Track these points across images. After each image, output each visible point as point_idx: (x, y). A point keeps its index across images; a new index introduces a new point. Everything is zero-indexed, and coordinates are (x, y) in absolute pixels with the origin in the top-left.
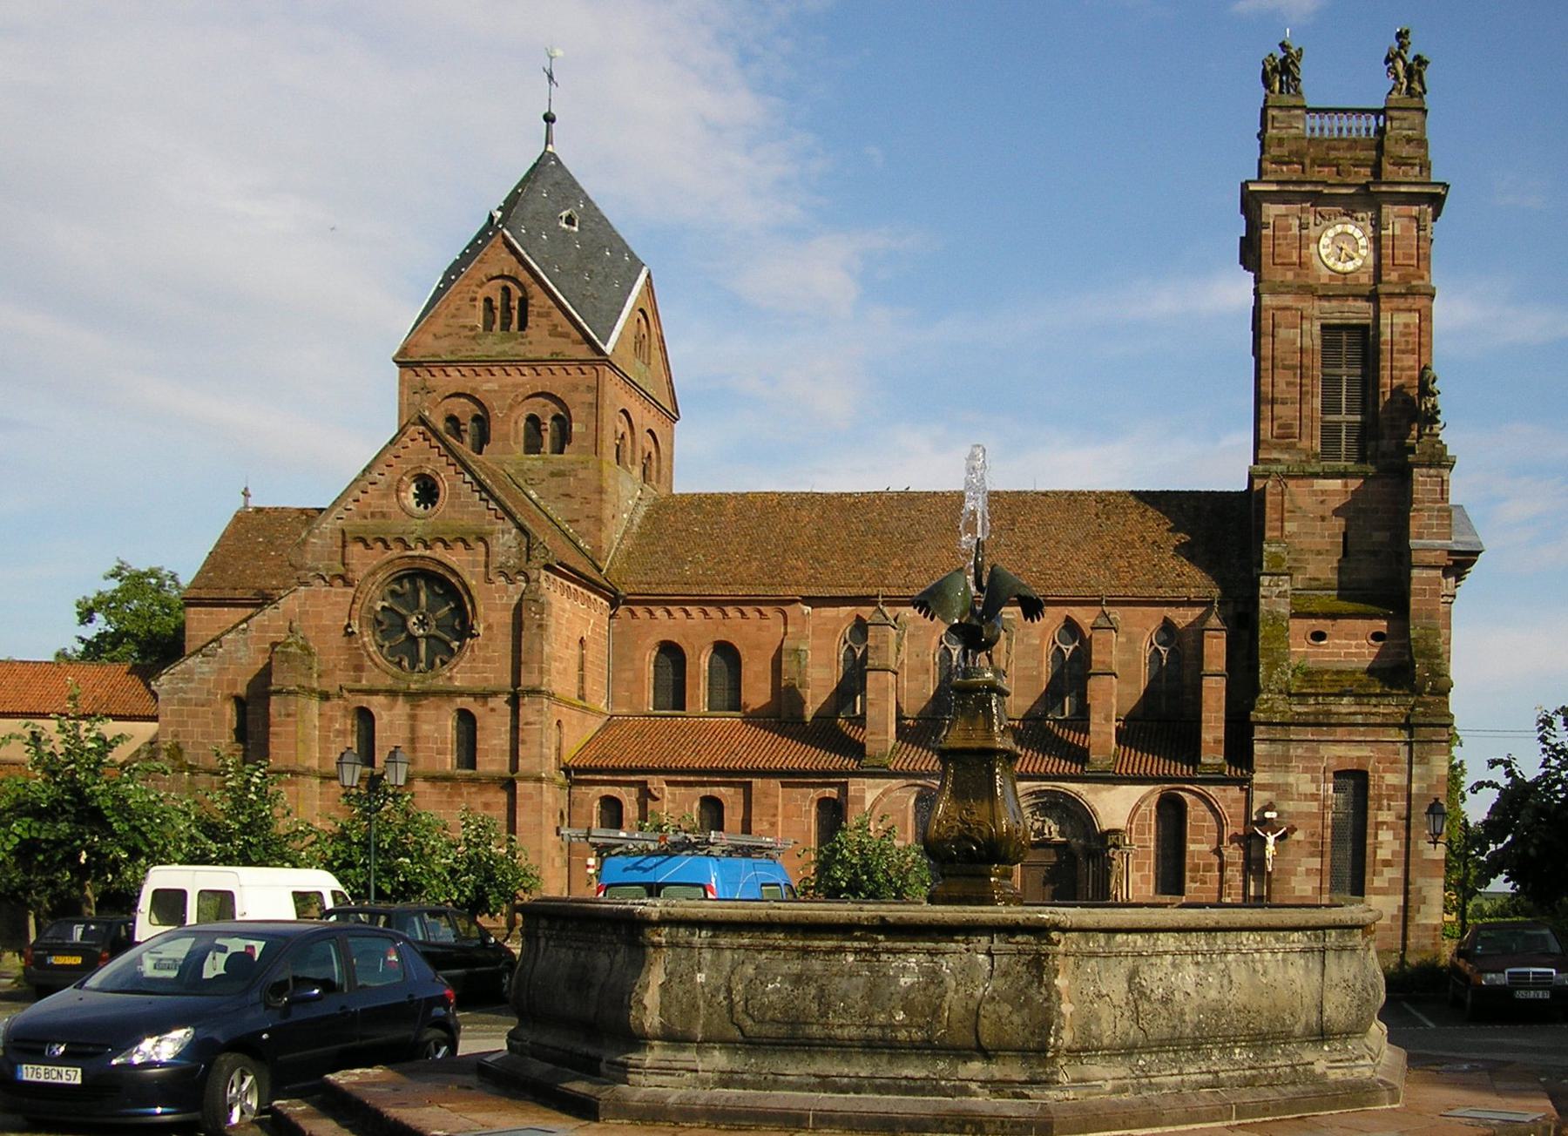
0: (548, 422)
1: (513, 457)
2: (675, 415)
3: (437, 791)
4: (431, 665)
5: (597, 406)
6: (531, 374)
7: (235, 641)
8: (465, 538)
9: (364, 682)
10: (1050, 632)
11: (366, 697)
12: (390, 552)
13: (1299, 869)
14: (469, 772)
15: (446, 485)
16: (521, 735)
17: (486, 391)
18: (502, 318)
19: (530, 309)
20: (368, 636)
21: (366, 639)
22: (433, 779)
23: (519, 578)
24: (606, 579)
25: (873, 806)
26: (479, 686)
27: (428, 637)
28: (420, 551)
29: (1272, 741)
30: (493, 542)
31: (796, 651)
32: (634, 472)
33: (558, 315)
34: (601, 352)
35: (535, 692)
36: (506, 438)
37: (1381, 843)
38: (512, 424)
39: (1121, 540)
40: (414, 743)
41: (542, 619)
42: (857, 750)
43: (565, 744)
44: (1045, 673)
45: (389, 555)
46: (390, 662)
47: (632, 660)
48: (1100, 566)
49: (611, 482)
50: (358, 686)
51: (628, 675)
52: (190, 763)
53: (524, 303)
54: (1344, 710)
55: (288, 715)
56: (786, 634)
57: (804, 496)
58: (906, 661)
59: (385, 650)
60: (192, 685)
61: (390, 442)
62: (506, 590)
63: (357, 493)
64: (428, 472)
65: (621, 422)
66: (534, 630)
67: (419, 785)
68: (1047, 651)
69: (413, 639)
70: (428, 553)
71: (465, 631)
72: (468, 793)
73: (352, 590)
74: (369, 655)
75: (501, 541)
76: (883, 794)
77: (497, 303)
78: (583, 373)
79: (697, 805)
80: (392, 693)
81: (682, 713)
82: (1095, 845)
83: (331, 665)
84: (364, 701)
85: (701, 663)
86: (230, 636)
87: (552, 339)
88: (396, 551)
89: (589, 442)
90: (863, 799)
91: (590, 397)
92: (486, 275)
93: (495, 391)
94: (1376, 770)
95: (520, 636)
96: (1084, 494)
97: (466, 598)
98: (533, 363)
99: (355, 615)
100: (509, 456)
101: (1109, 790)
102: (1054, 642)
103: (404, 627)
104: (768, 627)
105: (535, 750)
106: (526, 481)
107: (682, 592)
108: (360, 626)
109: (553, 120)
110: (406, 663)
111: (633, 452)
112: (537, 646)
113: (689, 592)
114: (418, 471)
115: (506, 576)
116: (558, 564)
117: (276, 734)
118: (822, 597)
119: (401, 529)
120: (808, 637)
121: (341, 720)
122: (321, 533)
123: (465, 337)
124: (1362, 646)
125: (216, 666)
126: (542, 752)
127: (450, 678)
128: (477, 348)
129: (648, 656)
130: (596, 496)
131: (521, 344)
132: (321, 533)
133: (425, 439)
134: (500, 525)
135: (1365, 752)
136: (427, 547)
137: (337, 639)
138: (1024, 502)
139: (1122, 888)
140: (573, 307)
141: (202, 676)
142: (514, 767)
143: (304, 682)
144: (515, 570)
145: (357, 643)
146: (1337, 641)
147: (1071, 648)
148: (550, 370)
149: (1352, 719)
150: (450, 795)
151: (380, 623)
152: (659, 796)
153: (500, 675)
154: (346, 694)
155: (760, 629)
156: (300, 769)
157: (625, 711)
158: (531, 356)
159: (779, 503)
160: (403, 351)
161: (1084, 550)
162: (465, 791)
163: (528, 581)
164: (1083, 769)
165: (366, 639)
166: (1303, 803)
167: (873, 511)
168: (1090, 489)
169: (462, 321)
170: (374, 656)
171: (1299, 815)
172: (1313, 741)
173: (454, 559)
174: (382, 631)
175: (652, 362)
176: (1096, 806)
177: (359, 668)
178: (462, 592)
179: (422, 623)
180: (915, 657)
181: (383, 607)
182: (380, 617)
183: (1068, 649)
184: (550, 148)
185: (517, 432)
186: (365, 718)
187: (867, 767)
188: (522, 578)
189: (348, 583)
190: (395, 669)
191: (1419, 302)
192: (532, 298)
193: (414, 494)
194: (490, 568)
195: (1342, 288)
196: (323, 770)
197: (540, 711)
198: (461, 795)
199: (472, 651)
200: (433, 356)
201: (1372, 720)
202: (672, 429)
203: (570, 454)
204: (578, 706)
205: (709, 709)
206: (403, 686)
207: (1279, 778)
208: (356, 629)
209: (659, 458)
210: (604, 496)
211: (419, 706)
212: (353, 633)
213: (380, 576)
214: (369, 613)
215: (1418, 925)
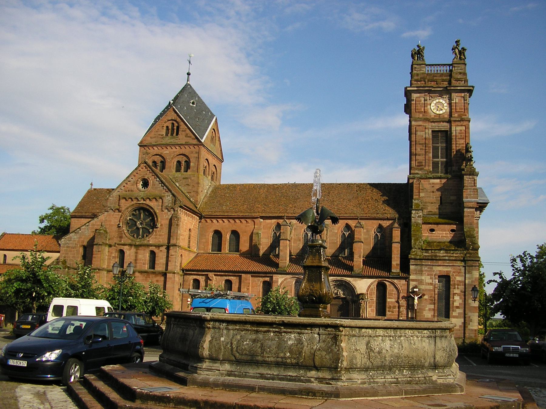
0: (183, 163)
4: (143, 237)
9: (122, 242)
10: (341, 228)
12: (133, 202)
13: (426, 308)
14: (152, 270)
16: (169, 259)
18: (171, 132)
19: (180, 129)
21: (124, 228)
22: (141, 272)
25: (281, 284)
26: (157, 244)
27: (143, 228)
28: (142, 202)
29: (416, 265)
31: (258, 233)
33: (188, 131)
34: (201, 142)
35: (175, 245)
36: (170, 167)
37: (455, 300)
38: (172, 163)
41: (178, 223)
42: (276, 265)
43: (183, 262)
44: (339, 241)
46: (131, 235)
48: (357, 207)
50: (120, 243)
51: (204, 240)
53: (178, 128)
54: (441, 255)
55: (99, 252)
56: (254, 228)
61: (135, 169)
63: (125, 184)
64: (146, 178)
66: (175, 226)
67: (137, 274)
68: (340, 234)
69: (138, 229)
70: (144, 202)
71: (154, 226)
72: (152, 277)
73: (121, 214)
74: (124, 233)
76: (284, 280)
77: (170, 128)
80: (130, 245)
81: (220, 253)
84: (122, 247)
85: (227, 237)
86: (83, 227)
88: (135, 202)
89: (195, 169)
91: (196, 155)
94: (453, 275)
96: (352, 184)
97: (155, 216)
98: (180, 145)
99: (121, 221)
101: (360, 280)
102: (342, 231)
103: (136, 225)
104: (249, 226)
108: (122, 224)
109: (190, 75)
110: (135, 236)
111: (209, 171)
114: (143, 178)
117: (95, 257)
118: (266, 216)
119: (137, 195)
121: (114, 253)
122: (113, 196)
124: (448, 234)
125: (78, 236)
130: (197, 185)
131: (177, 139)
132: (113, 196)
133: (146, 168)
134: (167, 194)
135: (449, 269)
136: (144, 200)
137: (115, 228)
138: (333, 187)
139: (364, 313)
142: (167, 269)
144: (171, 208)
146: (439, 232)
147: (348, 233)
149: (444, 258)
150: (146, 278)
151: (128, 224)
152: (212, 279)
153: (164, 240)
155: (246, 226)
156: (101, 268)
157: (202, 252)
158: (179, 143)
160: (141, 142)
161: (352, 202)
163: (174, 211)
164: (351, 273)
165: (124, 228)
166: (427, 286)
167: (283, 190)
168: (355, 183)
169: (159, 133)
170: (126, 234)
171: (426, 290)
172: (431, 265)
174: (129, 226)
178: (154, 214)
179: (141, 224)
181: (130, 219)
182: (128, 222)
183: (347, 234)
184: (188, 82)
185: (174, 166)
186: (122, 252)
187: (280, 271)
189: (120, 211)
190: (132, 238)
191: (465, 123)
192: (181, 126)
195: (439, 119)
196: (108, 269)
197: (176, 252)
198: (149, 278)
199: (156, 232)
200: (150, 143)
201: (451, 258)
202: (221, 164)
203: (189, 172)
206: (134, 243)
207: (419, 277)
209: (217, 173)
210: (199, 185)
211: (138, 249)
213: (129, 209)
215: (469, 329)
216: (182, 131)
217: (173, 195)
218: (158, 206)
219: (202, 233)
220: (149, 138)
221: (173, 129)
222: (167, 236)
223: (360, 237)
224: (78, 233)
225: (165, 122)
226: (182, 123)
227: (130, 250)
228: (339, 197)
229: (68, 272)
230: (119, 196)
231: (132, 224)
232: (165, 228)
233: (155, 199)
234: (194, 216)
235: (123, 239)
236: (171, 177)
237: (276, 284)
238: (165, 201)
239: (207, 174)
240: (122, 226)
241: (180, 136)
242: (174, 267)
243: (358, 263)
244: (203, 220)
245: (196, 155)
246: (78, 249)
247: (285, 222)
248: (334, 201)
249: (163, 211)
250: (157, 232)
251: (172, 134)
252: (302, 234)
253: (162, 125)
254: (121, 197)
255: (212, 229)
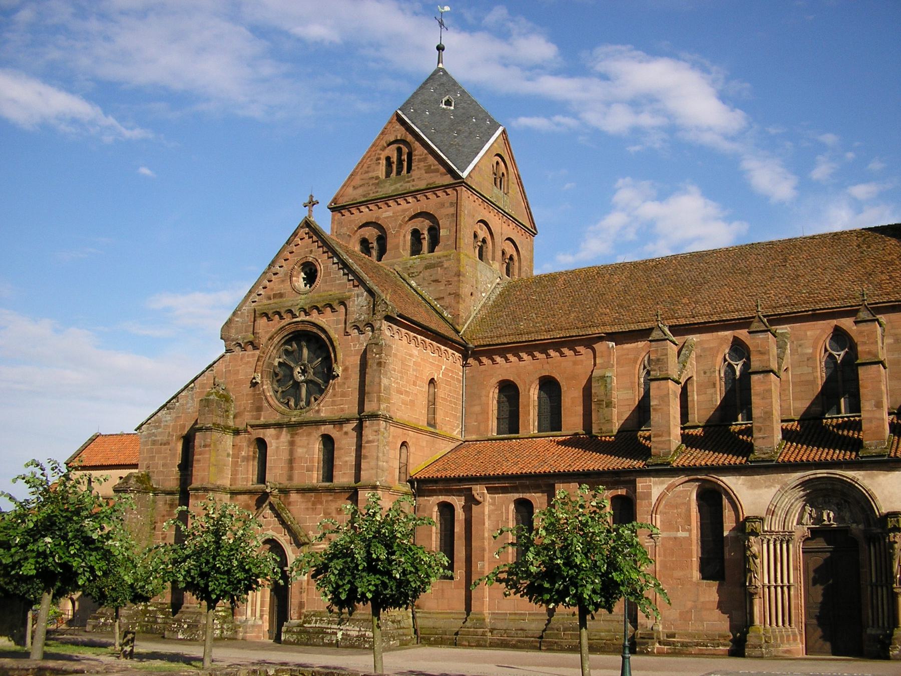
0: (426, 232)
1: (400, 260)
2: (533, 230)
3: (306, 500)
4: (308, 403)
5: (456, 215)
6: (414, 201)
7: (186, 396)
8: (332, 303)
9: (262, 419)
10: (821, 342)
11: (262, 430)
12: (283, 321)
14: (327, 484)
15: (322, 267)
16: (363, 452)
17: (385, 218)
18: (397, 168)
19: (413, 158)
20: (267, 384)
21: (265, 387)
22: (302, 491)
23: (367, 329)
24: (462, 338)
25: (659, 500)
26: (336, 416)
27: (307, 382)
28: (303, 317)
30: (350, 304)
31: (603, 378)
32: (494, 266)
33: (431, 159)
34: (460, 178)
35: (374, 416)
36: (397, 247)
38: (401, 238)
39: (882, 261)
40: (292, 464)
41: (380, 358)
42: (644, 452)
43: (411, 461)
44: (820, 376)
45: (284, 323)
46: (282, 403)
47: (480, 397)
48: (863, 282)
49: (468, 268)
50: (258, 422)
51: (477, 409)
52: (154, 486)
53: (410, 155)
55: (205, 446)
56: (595, 365)
57: (617, 266)
58: (695, 378)
59: (279, 394)
60: (160, 430)
61: (287, 243)
62: (359, 339)
63: (266, 282)
64: (311, 259)
65: (482, 230)
66: (375, 367)
67: (294, 496)
68: (821, 359)
69: (297, 385)
70: (307, 318)
71: (329, 374)
72: (326, 501)
73: (257, 352)
74: (266, 399)
75: (356, 303)
76: (668, 489)
77: (394, 159)
78: (448, 194)
79: (512, 507)
80: (279, 426)
81: (516, 435)
82: (877, 530)
83: (242, 408)
84: (260, 433)
86: (183, 394)
87: (427, 175)
88: (288, 319)
89: (451, 242)
90: (648, 495)
91: (452, 210)
92: (386, 142)
93: (390, 217)
95: (365, 373)
96: (846, 233)
97: (331, 349)
98: (414, 193)
99: (259, 369)
100: (398, 260)
102: (826, 350)
103: (292, 376)
104: (582, 361)
105: (373, 463)
106: (409, 275)
107: (515, 340)
108: (262, 378)
109: (443, 50)
110: (292, 403)
111: (494, 252)
112: (377, 380)
113: (521, 340)
114: (305, 260)
115: (357, 328)
116: (398, 316)
117: (199, 461)
118: (622, 332)
119: (290, 304)
120: (613, 366)
121: (246, 449)
122: (242, 313)
123: (373, 184)
125: (174, 415)
126: (377, 465)
127: (318, 411)
128: (380, 190)
129: (491, 394)
130: (456, 279)
131: (408, 182)
132: (242, 313)
133: (310, 237)
134: (357, 291)
136: (307, 314)
137: (246, 389)
138: (795, 246)
140: (441, 151)
141: (166, 423)
142: (358, 478)
143: (220, 421)
144: (364, 323)
145: (259, 390)
147: (842, 353)
148: (426, 196)
150: (314, 504)
151: (276, 375)
152: (481, 499)
153: (350, 408)
154: (249, 429)
155: (575, 363)
156: (210, 486)
157: (474, 437)
158: (413, 189)
159: (598, 273)
160: (335, 200)
161: (848, 272)
162: (324, 499)
163: (373, 331)
164: (857, 455)
165: (265, 387)
167: (670, 268)
168: (852, 229)
169: (371, 175)
170: (270, 399)
173: (324, 320)
174: (278, 381)
175: (510, 191)
176: (873, 490)
177: (259, 409)
178: (328, 343)
179: (304, 372)
180: (703, 375)
181: (279, 363)
182: (277, 370)
183: (840, 355)
184: (440, 65)
185: (404, 245)
186: (261, 444)
187: (652, 465)
188: (370, 328)
189: (255, 348)
190: (283, 408)
192: (415, 150)
193: (303, 278)
194: (348, 323)
196: (233, 487)
197: (377, 432)
198: (321, 503)
199: (334, 389)
200: (352, 200)
202: (532, 241)
203: (439, 251)
204: (427, 432)
205: (539, 431)
206: (286, 420)
208: (258, 380)
210: (461, 278)
211: (296, 434)
212: (257, 383)
213: (276, 340)
214: (268, 368)
216: (420, 161)
217: (371, 292)
218: (338, 322)
219: (471, 395)
220: (350, 190)
221: (400, 162)
222: (356, 396)
223: (872, 348)
224: (173, 408)
225: (383, 149)
226: (417, 144)
227: (278, 437)
228: (813, 264)
229: (154, 502)
230: (255, 311)
231: (285, 376)
232: (353, 375)
233: (330, 306)
234: (443, 347)
235: (262, 413)
236: (399, 269)
237: (645, 502)
238: (350, 309)
239: (490, 257)
240: (262, 382)
241: (415, 173)
242: (374, 471)
243: (874, 424)
244: (471, 361)
245: (452, 210)
246: (174, 445)
247: (660, 332)
248: (798, 276)
249: (347, 334)
250: (336, 387)
251: (399, 173)
252: (717, 368)
253: (377, 156)
254: (257, 312)
255: (494, 381)
